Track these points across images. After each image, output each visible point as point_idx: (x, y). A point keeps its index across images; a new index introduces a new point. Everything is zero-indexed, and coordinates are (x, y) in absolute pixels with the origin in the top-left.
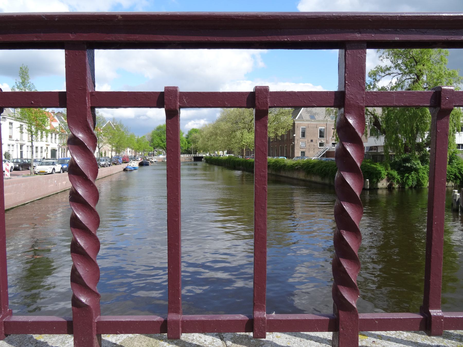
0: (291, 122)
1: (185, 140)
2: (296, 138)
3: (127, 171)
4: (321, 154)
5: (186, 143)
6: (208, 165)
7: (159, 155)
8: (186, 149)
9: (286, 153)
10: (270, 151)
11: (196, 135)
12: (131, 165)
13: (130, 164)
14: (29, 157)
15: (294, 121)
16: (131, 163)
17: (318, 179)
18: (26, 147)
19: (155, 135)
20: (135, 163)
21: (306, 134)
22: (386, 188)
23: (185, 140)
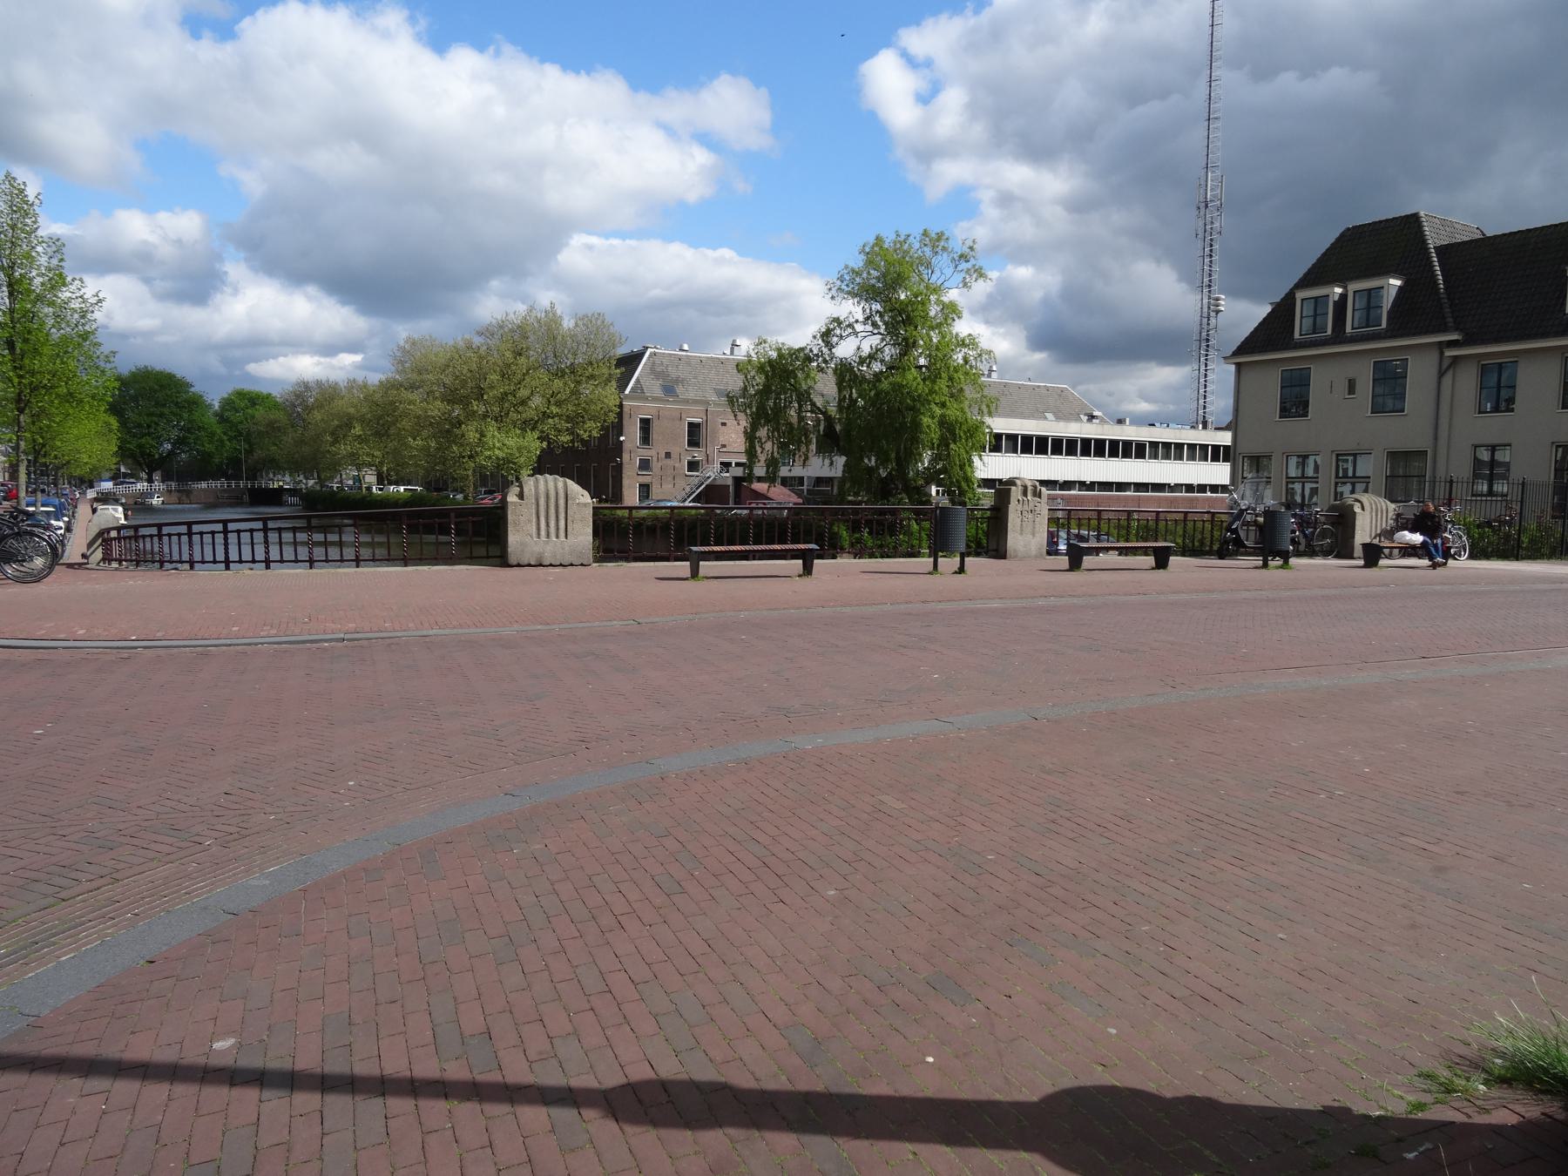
2: (626, 447)
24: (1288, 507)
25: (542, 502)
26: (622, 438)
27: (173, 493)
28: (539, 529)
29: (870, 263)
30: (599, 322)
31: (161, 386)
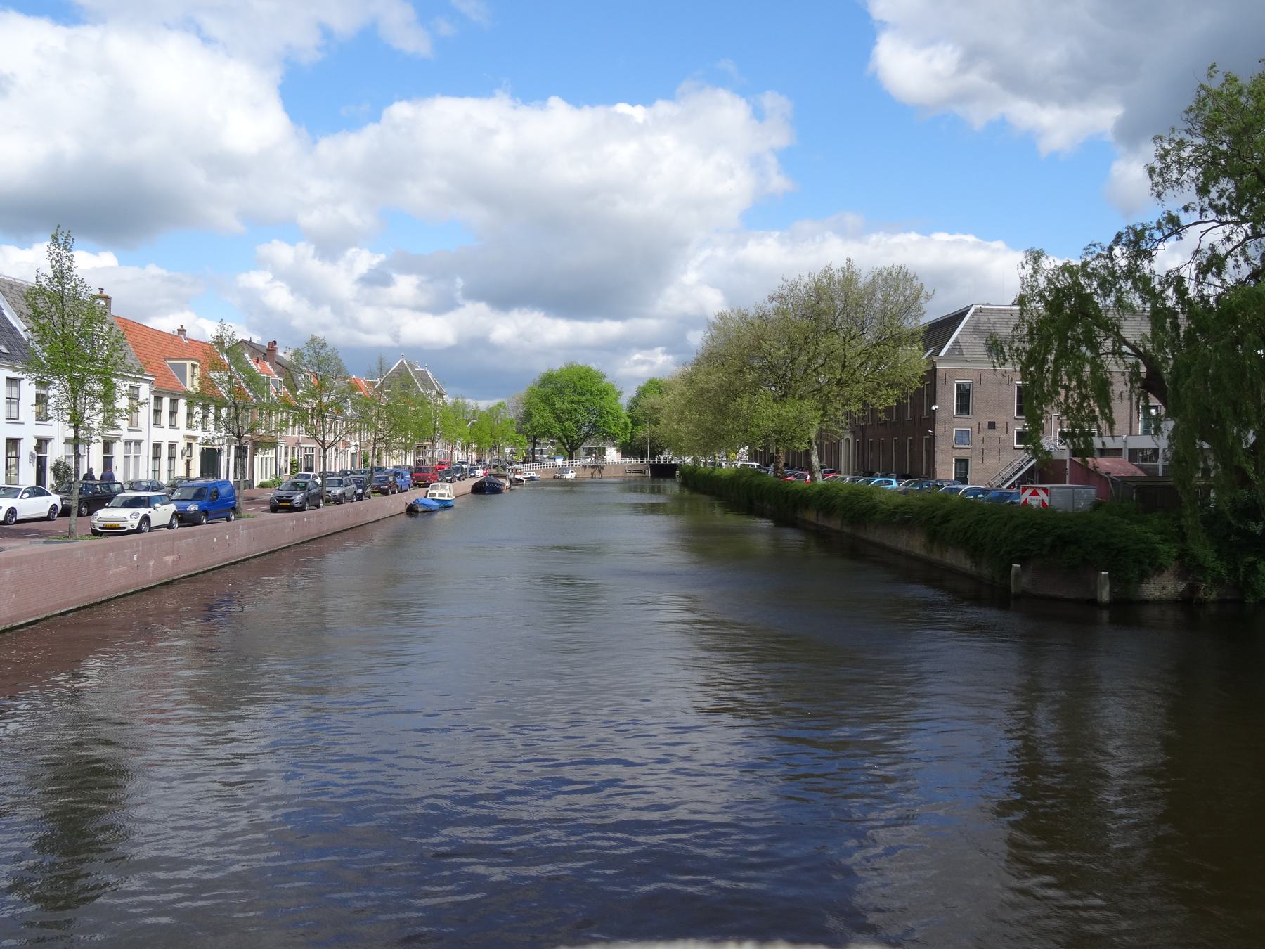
0: (923, 368)
1: (624, 412)
2: (940, 417)
3: (417, 512)
4: (1021, 469)
5: (625, 424)
6: (686, 493)
8: (628, 441)
9: (910, 462)
10: (866, 455)
11: (653, 400)
12: (434, 495)
13: (433, 492)
15: (934, 362)
17: (958, 560)
19: (535, 400)
20: (448, 487)
21: (974, 402)
22: (1176, 601)
24: (572, 419)
26: (934, 408)
29: (1209, 128)
30: (901, 277)
31: (581, 378)
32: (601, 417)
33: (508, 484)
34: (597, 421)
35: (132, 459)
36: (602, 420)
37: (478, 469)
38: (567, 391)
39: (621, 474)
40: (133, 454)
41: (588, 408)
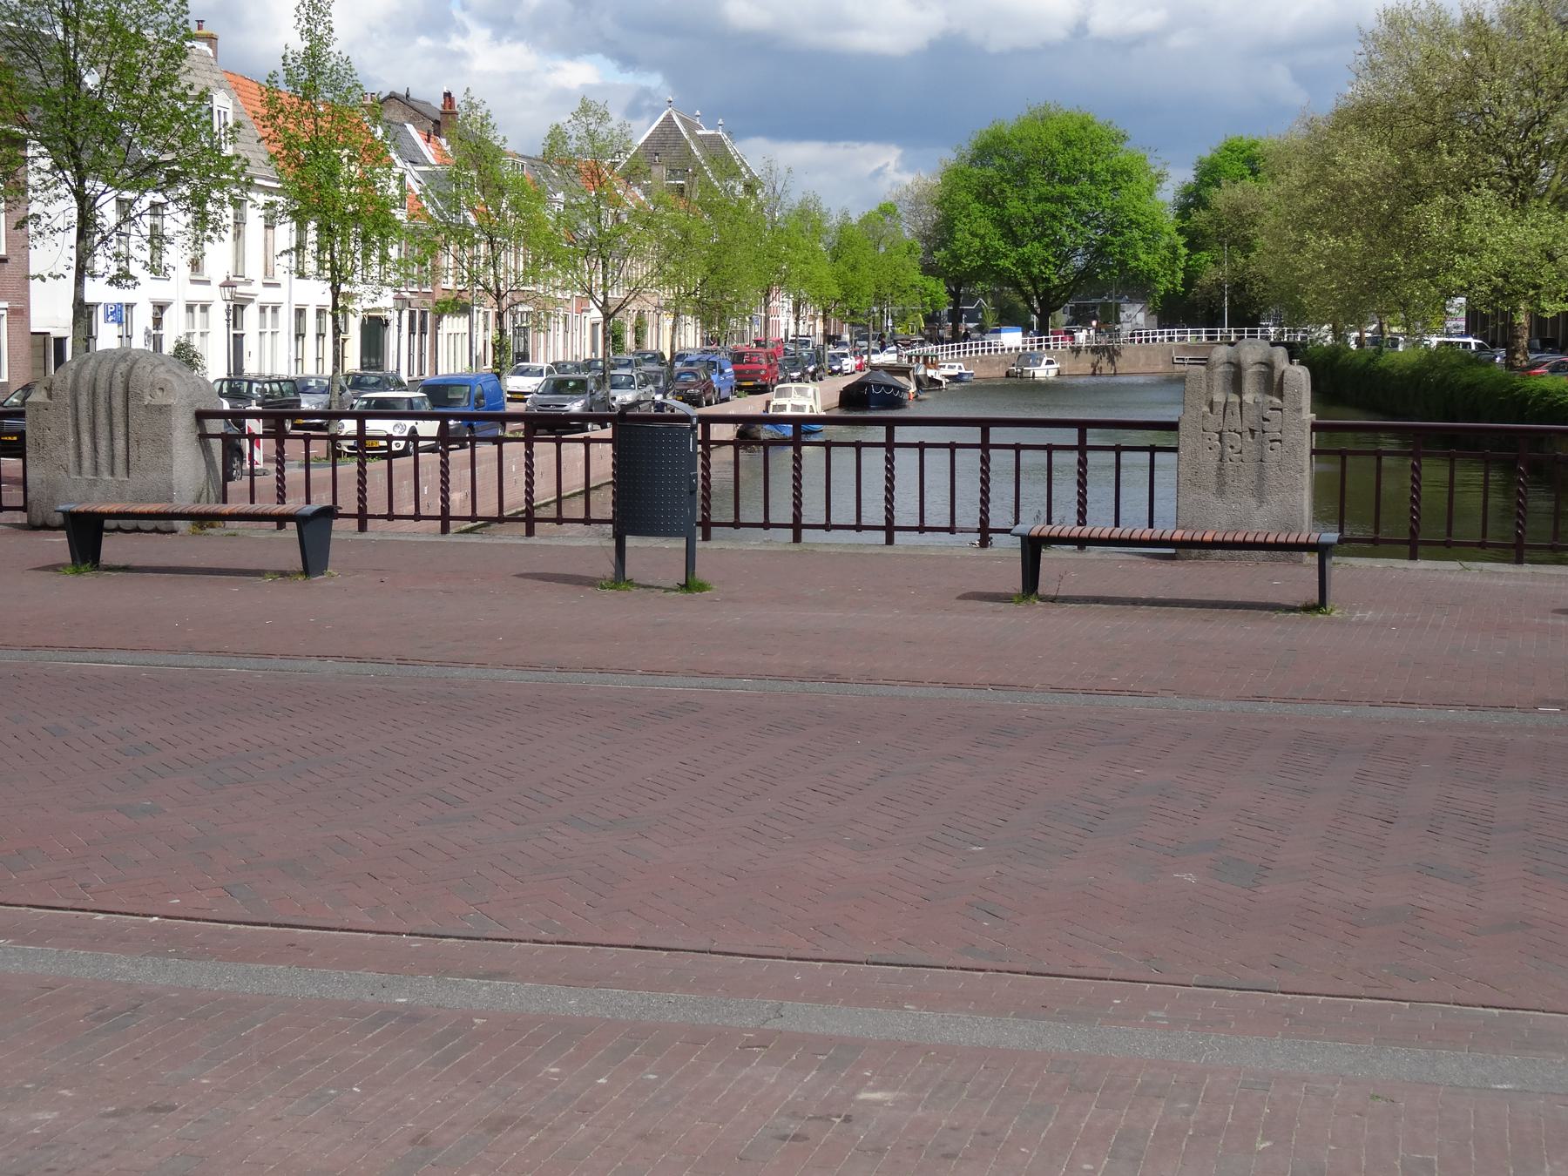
1: (1168, 220)
5: (1173, 249)
7: (999, 331)
14: (284, 369)
16: (781, 393)
18: (258, 310)
19: (963, 197)
20: (810, 392)
23: (1170, 228)
25: (84, 401)
27: (1082, 354)
28: (79, 456)
31: (1069, 143)
32: (1115, 234)
33: (913, 389)
34: (1105, 243)
35: (268, 336)
36: (1117, 240)
37: (845, 355)
38: (1036, 176)
39: (1160, 368)
40: (269, 329)
41: (1082, 213)
